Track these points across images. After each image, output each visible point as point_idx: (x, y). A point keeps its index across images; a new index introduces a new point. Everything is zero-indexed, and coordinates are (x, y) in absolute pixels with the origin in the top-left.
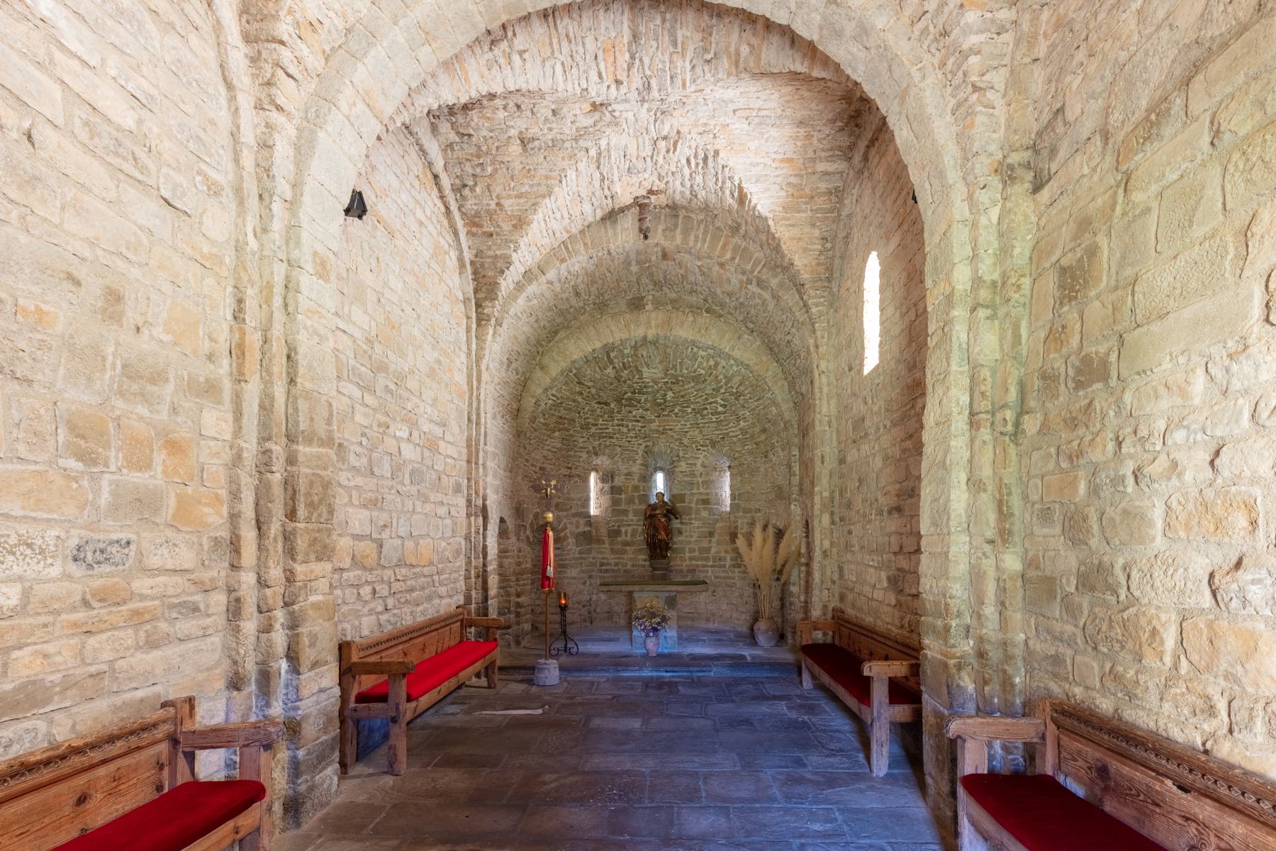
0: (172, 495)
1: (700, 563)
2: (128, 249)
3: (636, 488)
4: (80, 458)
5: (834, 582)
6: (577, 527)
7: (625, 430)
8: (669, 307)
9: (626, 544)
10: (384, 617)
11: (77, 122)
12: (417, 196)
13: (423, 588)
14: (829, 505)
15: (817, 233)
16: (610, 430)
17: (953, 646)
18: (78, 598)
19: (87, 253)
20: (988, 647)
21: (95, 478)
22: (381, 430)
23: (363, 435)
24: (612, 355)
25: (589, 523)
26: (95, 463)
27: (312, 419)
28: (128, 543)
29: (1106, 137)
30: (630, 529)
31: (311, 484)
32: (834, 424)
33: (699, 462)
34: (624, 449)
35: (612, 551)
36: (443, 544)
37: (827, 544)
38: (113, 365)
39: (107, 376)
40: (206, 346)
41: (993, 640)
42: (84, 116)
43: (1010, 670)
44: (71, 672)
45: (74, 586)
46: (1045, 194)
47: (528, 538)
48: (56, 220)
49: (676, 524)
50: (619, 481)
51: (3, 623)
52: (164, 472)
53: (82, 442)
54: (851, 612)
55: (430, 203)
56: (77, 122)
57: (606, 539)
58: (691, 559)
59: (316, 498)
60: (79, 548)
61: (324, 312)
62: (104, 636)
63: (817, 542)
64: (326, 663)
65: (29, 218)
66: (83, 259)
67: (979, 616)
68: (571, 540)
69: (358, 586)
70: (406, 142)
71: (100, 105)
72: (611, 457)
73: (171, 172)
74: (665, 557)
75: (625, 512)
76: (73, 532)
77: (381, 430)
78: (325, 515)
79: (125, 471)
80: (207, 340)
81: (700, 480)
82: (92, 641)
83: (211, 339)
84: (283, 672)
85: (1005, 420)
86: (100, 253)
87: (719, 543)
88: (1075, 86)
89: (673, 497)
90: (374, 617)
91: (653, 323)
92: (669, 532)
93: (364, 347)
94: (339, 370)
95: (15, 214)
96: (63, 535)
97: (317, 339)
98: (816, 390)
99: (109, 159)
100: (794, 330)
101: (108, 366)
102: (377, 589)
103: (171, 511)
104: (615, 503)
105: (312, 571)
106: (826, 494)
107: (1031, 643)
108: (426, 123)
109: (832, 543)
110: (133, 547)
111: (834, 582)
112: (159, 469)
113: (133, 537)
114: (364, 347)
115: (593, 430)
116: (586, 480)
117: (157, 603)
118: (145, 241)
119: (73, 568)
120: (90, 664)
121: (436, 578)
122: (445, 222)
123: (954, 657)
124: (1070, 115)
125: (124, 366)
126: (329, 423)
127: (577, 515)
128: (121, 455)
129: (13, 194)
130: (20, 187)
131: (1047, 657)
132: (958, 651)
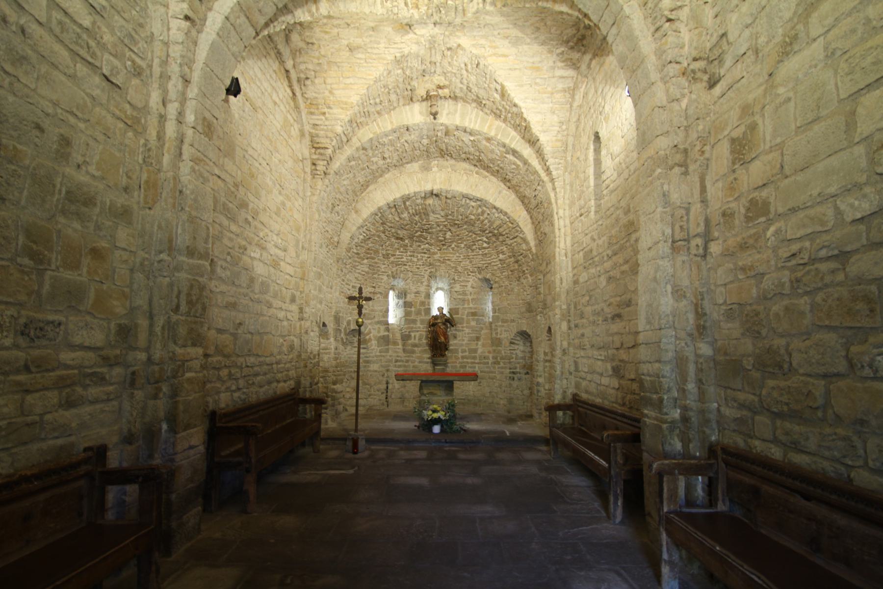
0: (93, 290)
1: (469, 361)
2: (78, 109)
3: (423, 303)
4: (32, 258)
5: (571, 373)
6: (379, 332)
7: (415, 260)
8: (450, 170)
9: (415, 345)
10: (236, 395)
11: (54, 22)
12: (274, 84)
13: (265, 374)
14: (566, 316)
15: (556, 118)
16: (404, 259)
17: (666, 414)
18: (22, 363)
19: (50, 111)
20: (691, 414)
21: (41, 273)
22: (241, 251)
23: (229, 254)
24: (408, 203)
25: (388, 330)
26: (41, 262)
27: (195, 238)
28: (60, 324)
29: (757, 52)
30: (417, 334)
31: (192, 286)
32: (569, 255)
33: (469, 284)
34: (414, 274)
35: (404, 350)
36: (281, 340)
37: (565, 344)
38: (60, 190)
39: (55, 199)
40: (124, 181)
41: (694, 408)
42: (58, 17)
43: (708, 431)
44: (13, 420)
45: (20, 354)
46: (718, 90)
47: (342, 339)
48: (33, 86)
49: (451, 331)
50: (410, 298)
51: (4, 353)
52: (88, 272)
53: (34, 247)
54: (584, 396)
55: (282, 90)
56: (54, 22)
57: (400, 342)
58: (463, 357)
59: (194, 298)
60: (26, 325)
61: (207, 160)
62: (37, 395)
63: (558, 343)
64: (195, 426)
65: (15, 84)
66: (48, 115)
67: (684, 391)
68: (374, 342)
69: (219, 369)
70: (268, 47)
71: (70, 11)
72: (405, 280)
73: (112, 58)
74: (443, 355)
75: (414, 321)
76: (23, 312)
77: (241, 251)
78: (200, 311)
79: (61, 269)
80: (125, 177)
81: (470, 298)
82: (29, 398)
83: (129, 177)
84: (163, 431)
85: (697, 245)
86: (59, 111)
87: (483, 345)
88: (734, 20)
89: (451, 311)
90: (229, 394)
91: (438, 181)
92: (446, 337)
93: (233, 189)
94: (215, 206)
95: (8, 80)
96: (16, 315)
97: (201, 180)
98: (557, 231)
99: (71, 46)
100: (539, 188)
101: (57, 191)
102: (233, 372)
103: (91, 302)
104: (407, 314)
105: (188, 353)
106: (564, 307)
107: (722, 409)
108: (283, 35)
109: (569, 344)
110: (62, 327)
111: (571, 373)
112: (85, 270)
113: (63, 319)
114: (233, 189)
115: (392, 259)
116: (387, 296)
117: (76, 371)
118: (89, 104)
119: (21, 341)
120: (28, 416)
121: (274, 366)
122: (292, 104)
123: (666, 422)
124: (731, 38)
125: (68, 192)
126: (206, 242)
127: (379, 322)
128: (59, 257)
129: (8, 68)
130: (13, 64)
131: (735, 420)
132: (668, 418)
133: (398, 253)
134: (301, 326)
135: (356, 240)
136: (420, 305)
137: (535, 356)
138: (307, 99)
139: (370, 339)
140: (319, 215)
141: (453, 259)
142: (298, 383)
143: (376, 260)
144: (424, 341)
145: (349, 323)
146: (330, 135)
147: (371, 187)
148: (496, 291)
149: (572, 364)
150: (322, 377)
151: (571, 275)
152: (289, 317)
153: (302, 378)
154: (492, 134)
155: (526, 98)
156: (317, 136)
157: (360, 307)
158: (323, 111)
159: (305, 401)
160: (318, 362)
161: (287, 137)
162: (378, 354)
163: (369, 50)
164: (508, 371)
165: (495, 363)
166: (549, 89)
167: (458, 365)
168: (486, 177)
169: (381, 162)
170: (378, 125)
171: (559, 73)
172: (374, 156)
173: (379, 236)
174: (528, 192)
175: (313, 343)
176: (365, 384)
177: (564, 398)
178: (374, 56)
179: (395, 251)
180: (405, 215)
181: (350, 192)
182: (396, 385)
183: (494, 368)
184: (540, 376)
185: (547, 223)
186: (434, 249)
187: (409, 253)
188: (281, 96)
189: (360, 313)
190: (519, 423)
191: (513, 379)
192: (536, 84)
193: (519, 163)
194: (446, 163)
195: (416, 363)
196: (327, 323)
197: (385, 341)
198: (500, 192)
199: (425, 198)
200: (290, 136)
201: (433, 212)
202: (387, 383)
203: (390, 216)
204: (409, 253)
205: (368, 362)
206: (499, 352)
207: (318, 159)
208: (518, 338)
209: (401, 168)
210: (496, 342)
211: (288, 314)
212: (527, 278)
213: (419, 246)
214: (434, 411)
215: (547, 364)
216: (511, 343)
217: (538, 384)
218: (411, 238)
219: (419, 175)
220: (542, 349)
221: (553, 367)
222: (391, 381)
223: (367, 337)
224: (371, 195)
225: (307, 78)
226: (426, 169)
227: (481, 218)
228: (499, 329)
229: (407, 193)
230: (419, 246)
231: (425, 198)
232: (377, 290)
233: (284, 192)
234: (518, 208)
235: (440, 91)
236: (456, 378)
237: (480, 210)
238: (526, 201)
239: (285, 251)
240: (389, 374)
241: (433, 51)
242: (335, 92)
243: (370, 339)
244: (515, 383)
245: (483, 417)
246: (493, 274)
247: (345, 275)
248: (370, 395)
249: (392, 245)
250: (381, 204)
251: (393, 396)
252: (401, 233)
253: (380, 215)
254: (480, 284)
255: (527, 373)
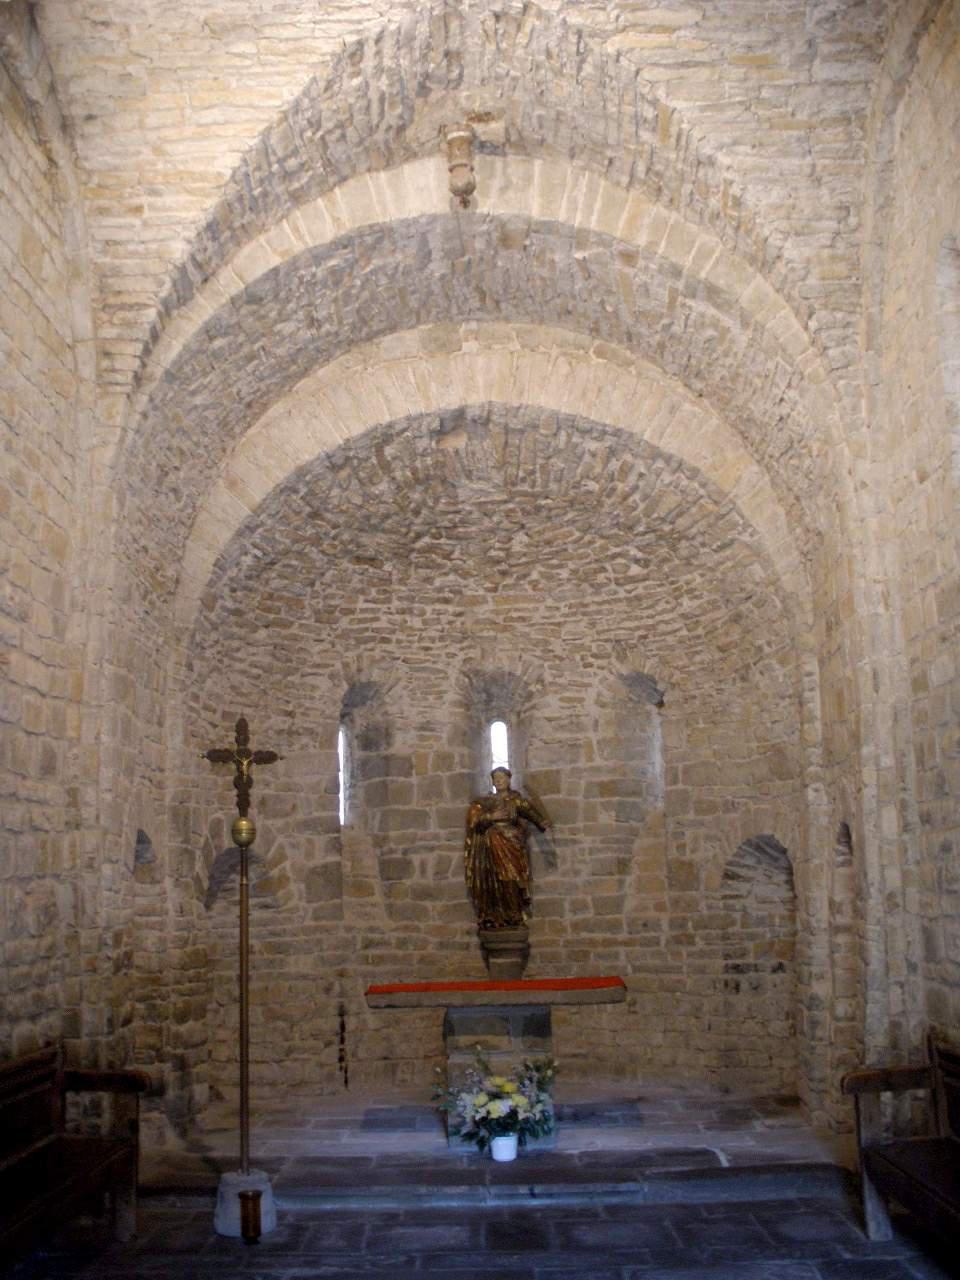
1: (598, 936)
6: (309, 855)
7: (417, 623)
8: (516, 346)
9: (425, 894)
16: (383, 623)
25: (337, 846)
32: (896, 600)
33: (590, 695)
37: (894, 877)
55: (20, 153)
57: (377, 883)
58: (576, 926)
63: (873, 874)
68: (296, 887)
81: (593, 737)
91: (480, 380)
100: (792, 394)
106: (887, 761)
111: (912, 967)
115: (344, 623)
116: (332, 744)
122: (47, 190)
127: (307, 825)
133: (361, 605)
134: (73, 845)
135: (233, 572)
136: (437, 767)
137: (801, 915)
138: (90, 173)
139: (283, 880)
140: (122, 504)
141: (537, 618)
142: (73, 1022)
143: (294, 630)
144: (458, 880)
145: (215, 831)
146: (154, 266)
147: (277, 409)
148: (673, 713)
149: (917, 936)
150: (141, 1000)
151: (904, 661)
152: (39, 821)
153: (84, 1006)
154: (642, 240)
155: (735, 143)
156: (117, 272)
157: (243, 785)
158: (136, 201)
159: (82, 1081)
160: (128, 955)
161: (27, 283)
162: (309, 923)
163: (267, 32)
164: (720, 963)
165: (677, 940)
166: (802, 116)
167: (563, 951)
168: (629, 363)
169: (306, 334)
170: (296, 230)
171: (822, 71)
172: (283, 318)
173: (300, 554)
174: (759, 408)
175: (110, 897)
176: (271, 1016)
177: (894, 1045)
178: (283, 47)
179: (352, 600)
180: (383, 487)
181: (212, 427)
182: (367, 1019)
183: (677, 955)
184: (821, 977)
185: (821, 500)
186: (473, 588)
187: (396, 604)
188: (16, 173)
189: (243, 805)
190: (758, 1126)
191: (737, 988)
192: (759, 101)
193: (727, 321)
194: (501, 328)
195: (430, 949)
196: (150, 832)
197: (329, 881)
198: (673, 409)
199: (440, 433)
200: (40, 282)
201: (469, 475)
202: (342, 1013)
203: (335, 492)
204: (396, 604)
205: (278, 949)
206: (691, 906)
207: (119, 339)
208: (750, 861)
209: (367, 348)
210: (683, 875)
211: (36, 810)
212: (769, 668)
213: (428, 580)
214: (496, 1096)
215: (841, 939)
216: (728, 876)
217: (813, 1002)
218: (402, 554)
219: (424, 366)
220: (823, 889)
221: (859, 950)
222: (352, 1008)
223: (275, 872)
224: (274, 432)
225: (90, 118)
226: (447, 346)
227: (620, 486)
228: (689, 833)
229: (386, 419)
230: (428, 580)
231: (440, 433)
232: (299, 721)
233: (19, 444)
234: (730, 455)
235: (479, 128)
236: (559, 996)
237: (614, 465)
238: (754, 434)
239: (23, 618)
240: (348, 983)
241: (454, 25)
242: (168, 147)
243: (283, 880)
244: (742, 1001)
245: (644, 1110)
246: (664, 662)
247: (202, 679)
248: (289, 1051)
249: (342, 580)
250: (306, 457)
251: (362, 1054)
252: (372, 542)
253: (304, 496)
254: (624, 692)
255: (779, 968)
